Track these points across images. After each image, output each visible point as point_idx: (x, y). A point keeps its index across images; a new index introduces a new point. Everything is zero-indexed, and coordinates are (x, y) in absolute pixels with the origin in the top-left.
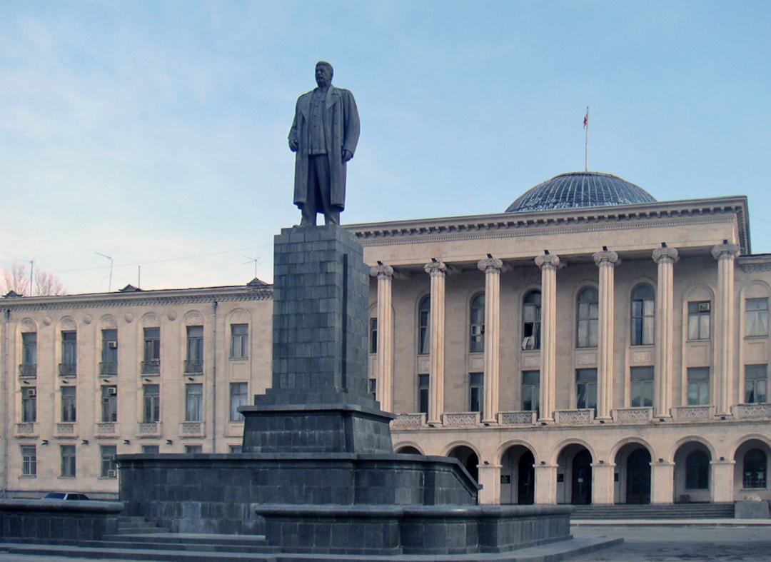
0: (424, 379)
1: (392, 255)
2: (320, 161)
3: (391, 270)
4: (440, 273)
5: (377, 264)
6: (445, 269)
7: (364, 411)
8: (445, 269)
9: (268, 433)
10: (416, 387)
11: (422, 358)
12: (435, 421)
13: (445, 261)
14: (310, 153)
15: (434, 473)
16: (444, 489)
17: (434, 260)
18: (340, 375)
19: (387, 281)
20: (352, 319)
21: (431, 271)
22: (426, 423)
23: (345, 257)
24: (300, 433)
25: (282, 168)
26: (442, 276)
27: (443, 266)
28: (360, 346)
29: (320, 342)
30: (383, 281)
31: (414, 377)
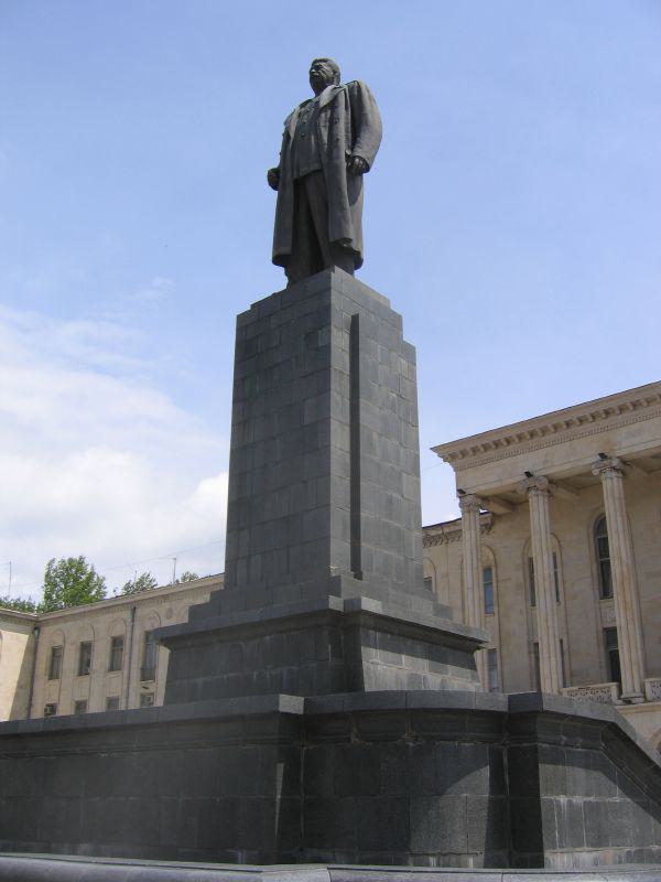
0: (610, 635)
1: (545, 462)
2: (311, 186)
3: (545, 481)
4: (614, 474)
5: (525, 477)
6: (621, 466)
7: (392, 614)
8: (621, 466)
9: (200, 681)
10: (602, 649)
11: (605, 603)
12: (634, 695)
13: (618, 455)
14: (295, 176)
15: (536, 748)
16: (578, 800)
17: (603, 456)
18: (347, 545)
19: (541, 498)
20: (375, 435)
21: (601, 472)
22: (619, 698)
23: (355, 319)
24: (255, 674)
25: (258, 211)
26: (618, 477)
27: (615, 463)
28: (399, 491)
29: (304, 482)
30: (535, 498)
31: (597, 632)
